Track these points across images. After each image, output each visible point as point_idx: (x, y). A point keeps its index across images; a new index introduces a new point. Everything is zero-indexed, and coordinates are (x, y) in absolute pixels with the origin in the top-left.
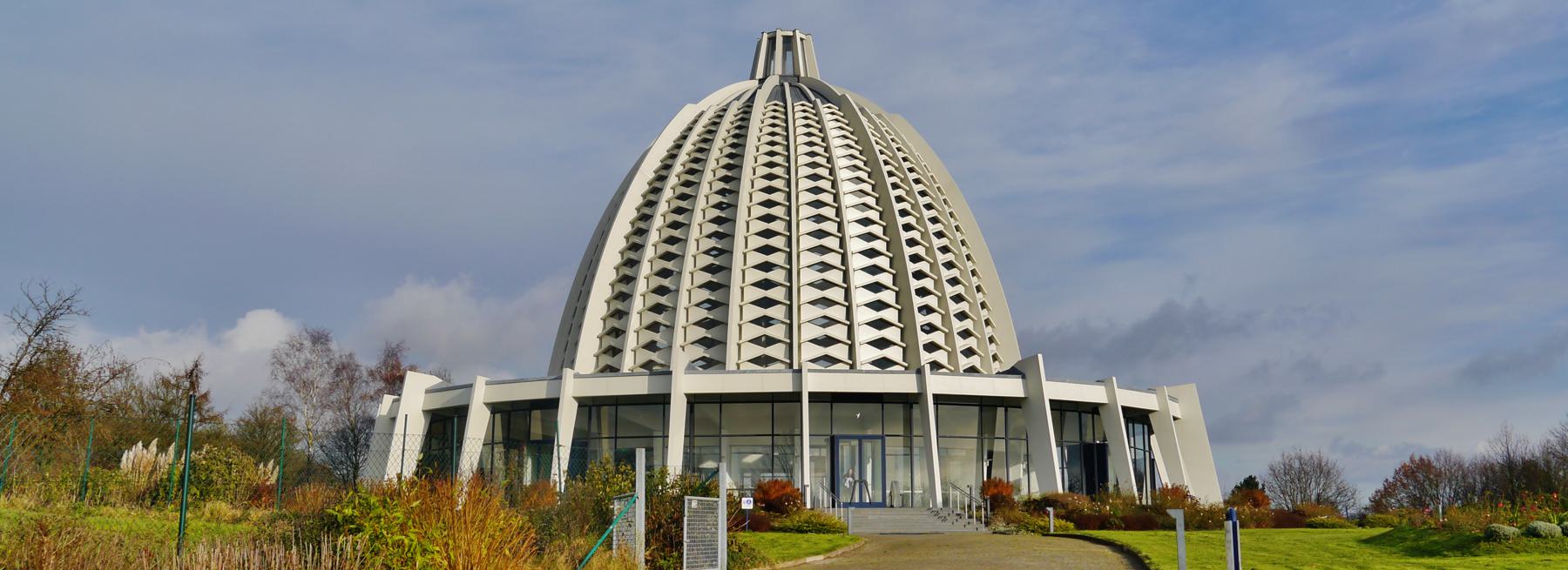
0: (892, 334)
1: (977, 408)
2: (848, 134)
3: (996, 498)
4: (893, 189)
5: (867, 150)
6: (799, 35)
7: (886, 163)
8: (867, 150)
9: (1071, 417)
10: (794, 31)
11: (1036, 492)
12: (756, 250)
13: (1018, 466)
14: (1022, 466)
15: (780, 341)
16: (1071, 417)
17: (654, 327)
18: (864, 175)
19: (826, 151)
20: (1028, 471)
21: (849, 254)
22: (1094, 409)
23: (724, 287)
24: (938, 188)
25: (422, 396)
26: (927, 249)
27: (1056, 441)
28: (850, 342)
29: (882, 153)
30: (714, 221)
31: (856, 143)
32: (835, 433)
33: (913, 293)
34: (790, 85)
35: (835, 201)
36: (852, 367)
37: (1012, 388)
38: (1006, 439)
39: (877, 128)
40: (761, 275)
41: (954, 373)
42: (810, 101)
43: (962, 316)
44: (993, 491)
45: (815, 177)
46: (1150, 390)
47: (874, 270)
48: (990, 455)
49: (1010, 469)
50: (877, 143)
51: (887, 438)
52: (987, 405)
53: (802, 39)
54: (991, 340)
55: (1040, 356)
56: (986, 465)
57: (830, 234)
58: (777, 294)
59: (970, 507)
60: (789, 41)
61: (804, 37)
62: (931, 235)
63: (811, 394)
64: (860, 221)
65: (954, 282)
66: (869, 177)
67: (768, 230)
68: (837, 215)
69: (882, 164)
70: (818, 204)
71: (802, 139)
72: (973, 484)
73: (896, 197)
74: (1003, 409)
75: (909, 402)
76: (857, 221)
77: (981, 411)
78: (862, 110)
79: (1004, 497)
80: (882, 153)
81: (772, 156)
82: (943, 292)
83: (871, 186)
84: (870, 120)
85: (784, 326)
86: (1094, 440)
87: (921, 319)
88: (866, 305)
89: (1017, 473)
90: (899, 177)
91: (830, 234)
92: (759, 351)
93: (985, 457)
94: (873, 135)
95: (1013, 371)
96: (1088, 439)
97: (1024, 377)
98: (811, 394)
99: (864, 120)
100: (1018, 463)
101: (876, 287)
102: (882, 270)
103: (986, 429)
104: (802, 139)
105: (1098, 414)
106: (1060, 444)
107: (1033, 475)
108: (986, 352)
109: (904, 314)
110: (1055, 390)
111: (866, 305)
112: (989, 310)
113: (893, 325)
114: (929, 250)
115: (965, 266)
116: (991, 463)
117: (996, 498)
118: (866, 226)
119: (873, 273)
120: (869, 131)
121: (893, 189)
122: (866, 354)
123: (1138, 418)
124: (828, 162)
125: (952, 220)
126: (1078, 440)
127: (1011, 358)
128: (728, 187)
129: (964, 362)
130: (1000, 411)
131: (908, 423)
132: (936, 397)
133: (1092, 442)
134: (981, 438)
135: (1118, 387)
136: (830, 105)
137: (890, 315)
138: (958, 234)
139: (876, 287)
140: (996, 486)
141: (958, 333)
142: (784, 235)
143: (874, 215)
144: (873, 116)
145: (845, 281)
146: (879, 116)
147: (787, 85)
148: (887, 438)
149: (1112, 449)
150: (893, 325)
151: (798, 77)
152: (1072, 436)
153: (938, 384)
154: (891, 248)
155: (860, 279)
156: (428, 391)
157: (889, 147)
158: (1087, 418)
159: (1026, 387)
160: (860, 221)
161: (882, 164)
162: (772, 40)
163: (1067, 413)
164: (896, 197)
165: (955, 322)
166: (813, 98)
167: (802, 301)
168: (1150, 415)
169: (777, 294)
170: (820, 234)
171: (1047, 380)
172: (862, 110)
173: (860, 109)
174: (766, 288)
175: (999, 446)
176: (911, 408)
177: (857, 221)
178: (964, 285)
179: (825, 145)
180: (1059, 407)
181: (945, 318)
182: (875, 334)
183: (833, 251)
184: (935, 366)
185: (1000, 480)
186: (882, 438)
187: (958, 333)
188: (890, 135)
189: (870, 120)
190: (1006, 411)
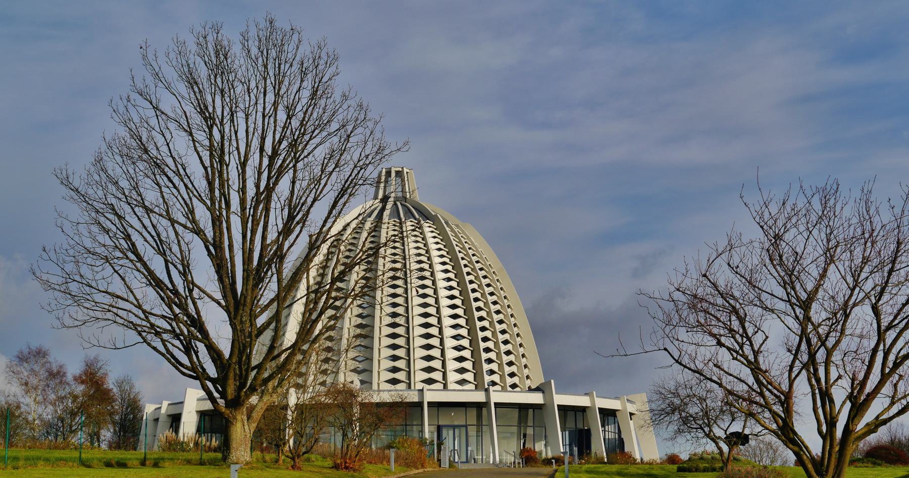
0: (468, 365)
1: (517, 410)
2: (437, 235)
3: (528, 457)
4: (467, 275)
5: (451, 252)
6: (405, 170)
7: (463, 259)
8: (451, 252)
9: (571, 415)
10: (402, 168)
11: (550, 455)
12: (387, 325)
13: (541, 442)
14: (543, 442)
15: (403, 382)
16: (571, 415)
17: (326, 360)
18: (447, 260)
19: (425, 246)
20: (546, 445)
21: (437, 280)
22: (583, 409)
23: (370, 348)
24: (490, 265)
25: (195, 402)
26: (485, 303)
27: (561, 428)
28: (443, 370)
29: (460, 252)
30: (360, 316)
31: (442, 240)
32: (440, 424)
33: (476, 319)
34: (401, 204)
35: (433, 285)
36: (445, 386)
37: (537, 398)
38: (534, 427)
39: (456, 236)
40: (391, 331)
41: (504, 389)
42: (415, 219)
43: (503, 332)
44: (526, 454)
45: (426, 315)
46: (617, 398)
47: (455, 316)
48: (525, 436)
49: (536, 445)
50: (457, 246)
51: (468, 427)
52: (523, 408)
53: (407, 173)
54: (521, 345)
55: (552, 381)
56: (522, 441)
57: (431, 305)
58: (400, 320)
59: (514, 463)
60: (399, 174)
61: (408, 171)
62: (493, 313)
63: (429, 403)
64: (456, 348)
65: (503, 332)
66: (453, 269)
67: (394, 333)
68: (435, 294)
69: (460, 259)
70: (427, 325)
71: (416, 274)
72: (515, 450)
73: (471, 290)
74: (532, 410)
75: (479, 407)
76: (448, 307)
77: (520, 411)
78: (447, 223)
79: (532, 457)
80: (460, 252)
81: (394, 338)
82: (492, 318)
83: (459, 292)
84: (452, 230)
85: (405, 373)
86: (584, 427)
87: (484, 356)
88: (449, 316)
89: (540, 446)
90: (470, 268)
91: (431, 305)
92: (391, 376)
93: (522, 437)
94: (454, 240)
95: (538, 389)
96: (580, 426)
97: (543, 392)
98: (495, 404)
99: (447, 229)
100: (541, 440)
101: (459, 348)
102: (465, 348)
103: (522, 421)
104: (416, 274)
105: (585, 412)
106: (563, 430)
107: (549, 448)
108: (520, 363)
109: (473, 342)
110: (561, 399)
111: (449, 316)
112: (521, 337)
113: (468, 360)
114: (483, 295)
115: (507, 312)
116: (525, 441)
117: (528, 457)
118: (453, 309)
119: (460, 361)
120: (452, 238)
121: (467, 275)
122: (453, 377)
123: (608, 415)
124: (428, 260)
125: (498, 284)
126: (574, 427)
127: (538, 379)
128: (364, 323)
129: (510, 381)
130: (531, 411)
131: (479, 417)
132: (495, 404)
133: (582, 428)
134: (519, 426)
135: (556, 394)
136: (428, 221)
137: (468, 365)
138: (502, 292)
139: (459, 348)
140: (528, 451)
141: (499, 332)
142: (403, 287)
143: (454, 284)
144: (453, 226)
145: (440, 334)
146: (457, 226)
147: (399, 204)
148: (468, 427)
149: (593, 432)
150: (468, 360)
151: (406, 198)
152: (571, 424)
153: (497, 396)
154: (467, 313)
155: (447, 322)
156: (198, 400)
157: (464, 248)
158: (579, 414)
159: (545, 398)
160: (456, 348)
161: (460, 259)
162: (389, 173)
163: (569, 412)
164: (471, 290)
165: (506, 367)
166: (417, 216)
167: (416, 380)
168: (617, 413)
169: (400, 331)
170: (429, 358)
171: (556, 394)
172: (447, 223)
173: (446, 222)
174: (394, 379)
175: (530, 431)
176: (482, 410)
177: (448, 307)
178: (506, 324)
179: (426, 249)
180: (564, 410)
181: (496, 344)
182: (458, 365)
183: (431, 305)
184: (494, 383)
185: (530, 449)
186: (466, 426)
187: (499, 332)
188: (465, 239)
189: (452, 230)
190: (534, 411)
